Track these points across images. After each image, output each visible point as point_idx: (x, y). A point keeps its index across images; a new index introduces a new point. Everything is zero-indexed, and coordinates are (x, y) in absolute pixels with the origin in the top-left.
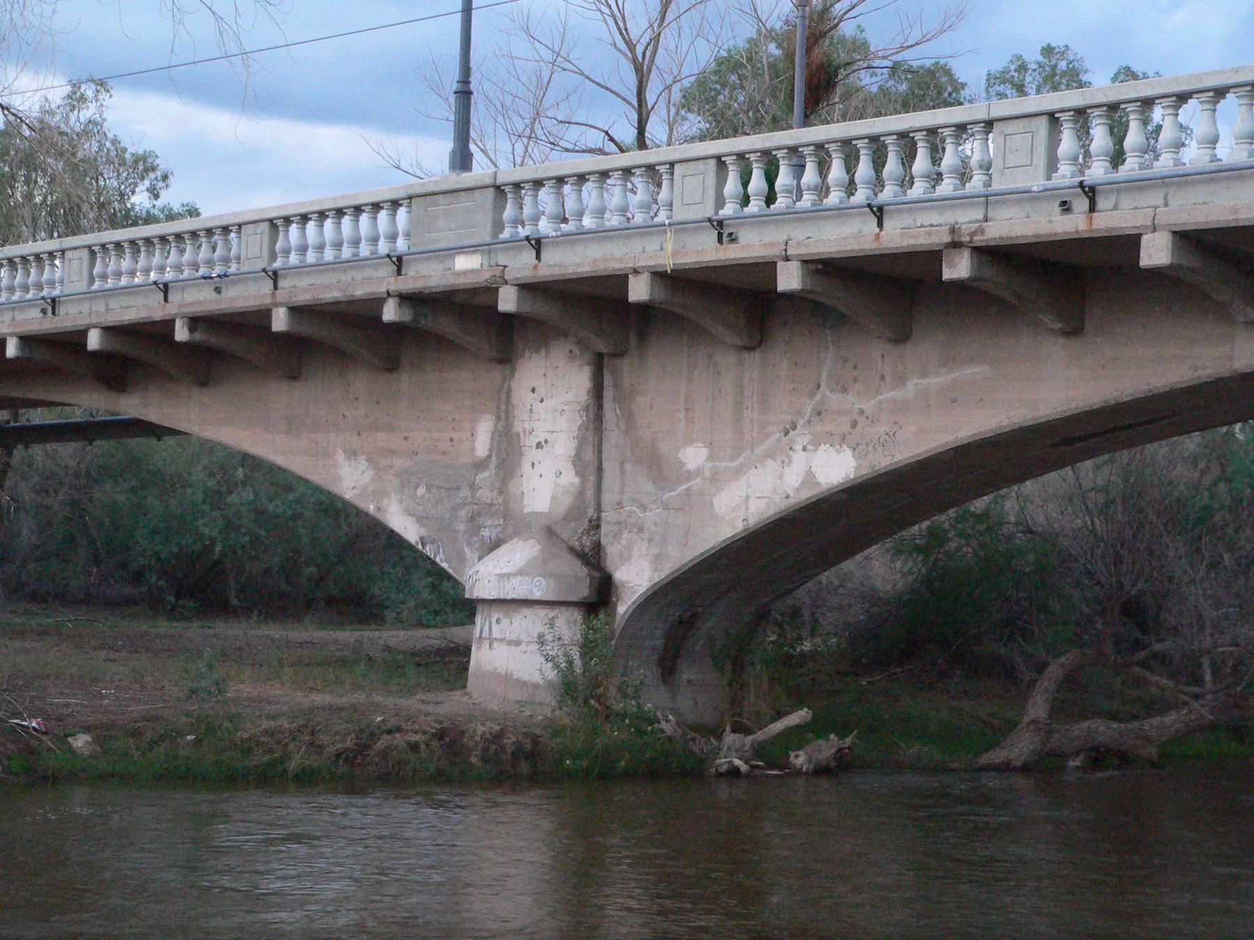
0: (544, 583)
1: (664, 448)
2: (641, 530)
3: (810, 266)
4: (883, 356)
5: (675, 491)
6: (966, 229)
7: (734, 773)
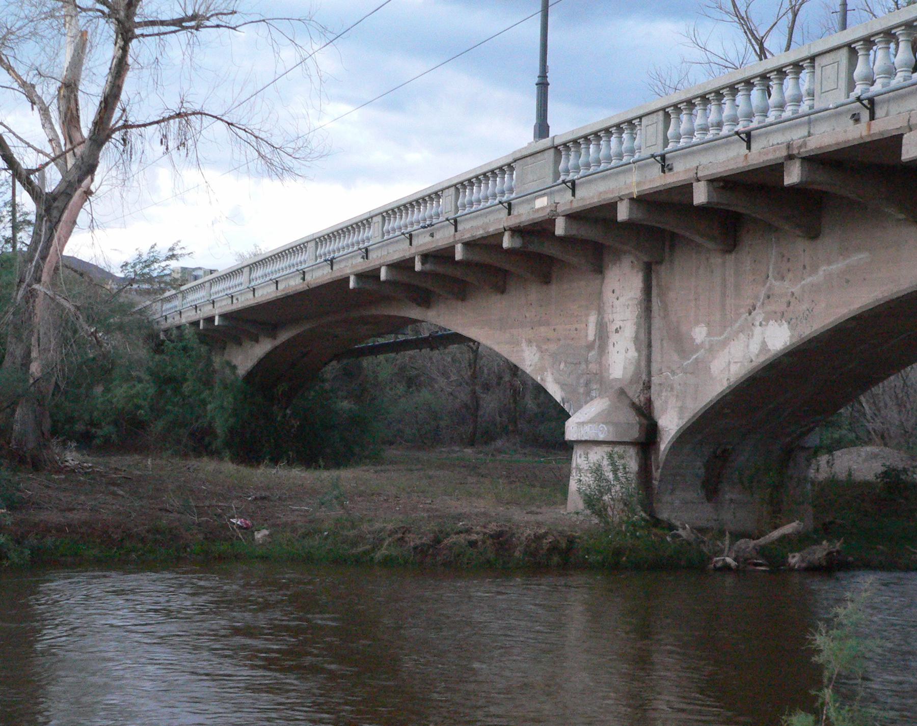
0: (606, 429)
1: (684, 329)
2: (672, 389)
3: (715, 184)
4: (804, 251)
5: (689, 360)
6: (796, 144)
7: (726, 568)
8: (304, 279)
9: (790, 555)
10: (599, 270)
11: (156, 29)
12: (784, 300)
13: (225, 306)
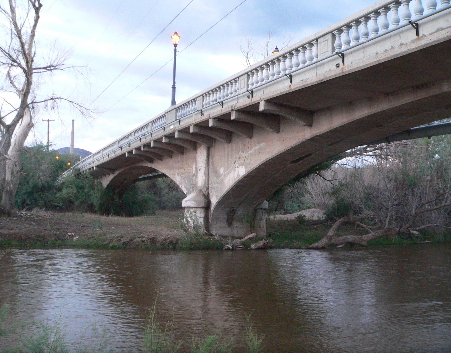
7: (229, 249)
8: (115, 154)
9: (252, 244)
10: (195, 149)
11: (40, 70)
12: (244, 159)
13: (97, 163)
